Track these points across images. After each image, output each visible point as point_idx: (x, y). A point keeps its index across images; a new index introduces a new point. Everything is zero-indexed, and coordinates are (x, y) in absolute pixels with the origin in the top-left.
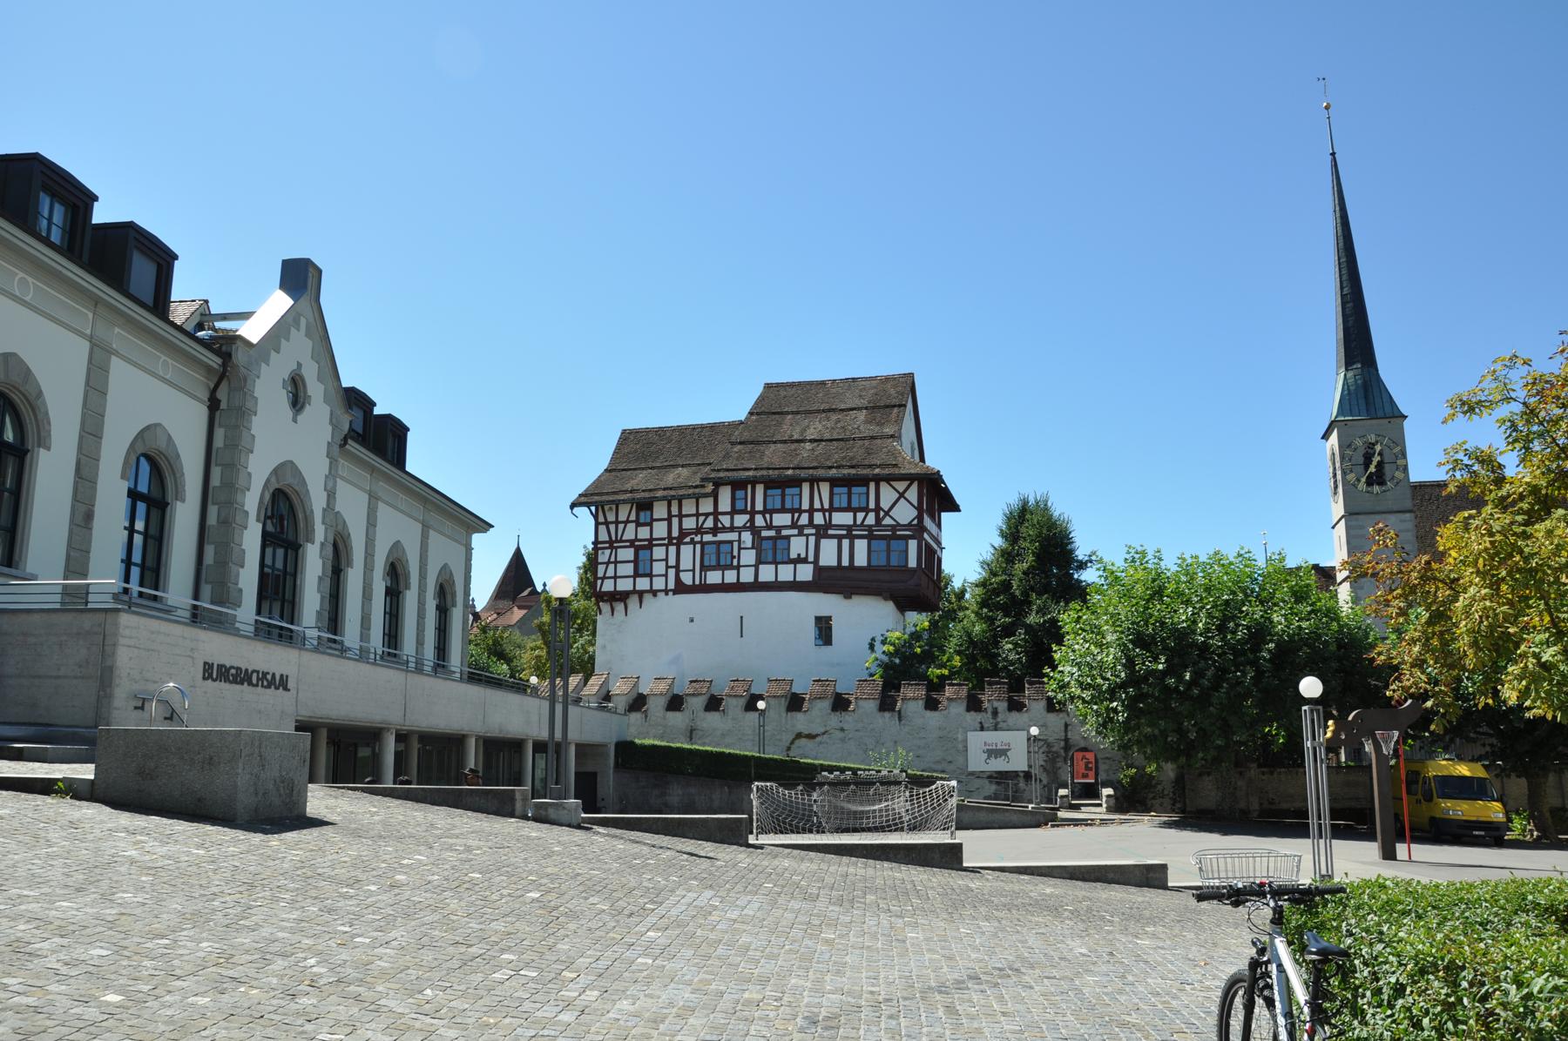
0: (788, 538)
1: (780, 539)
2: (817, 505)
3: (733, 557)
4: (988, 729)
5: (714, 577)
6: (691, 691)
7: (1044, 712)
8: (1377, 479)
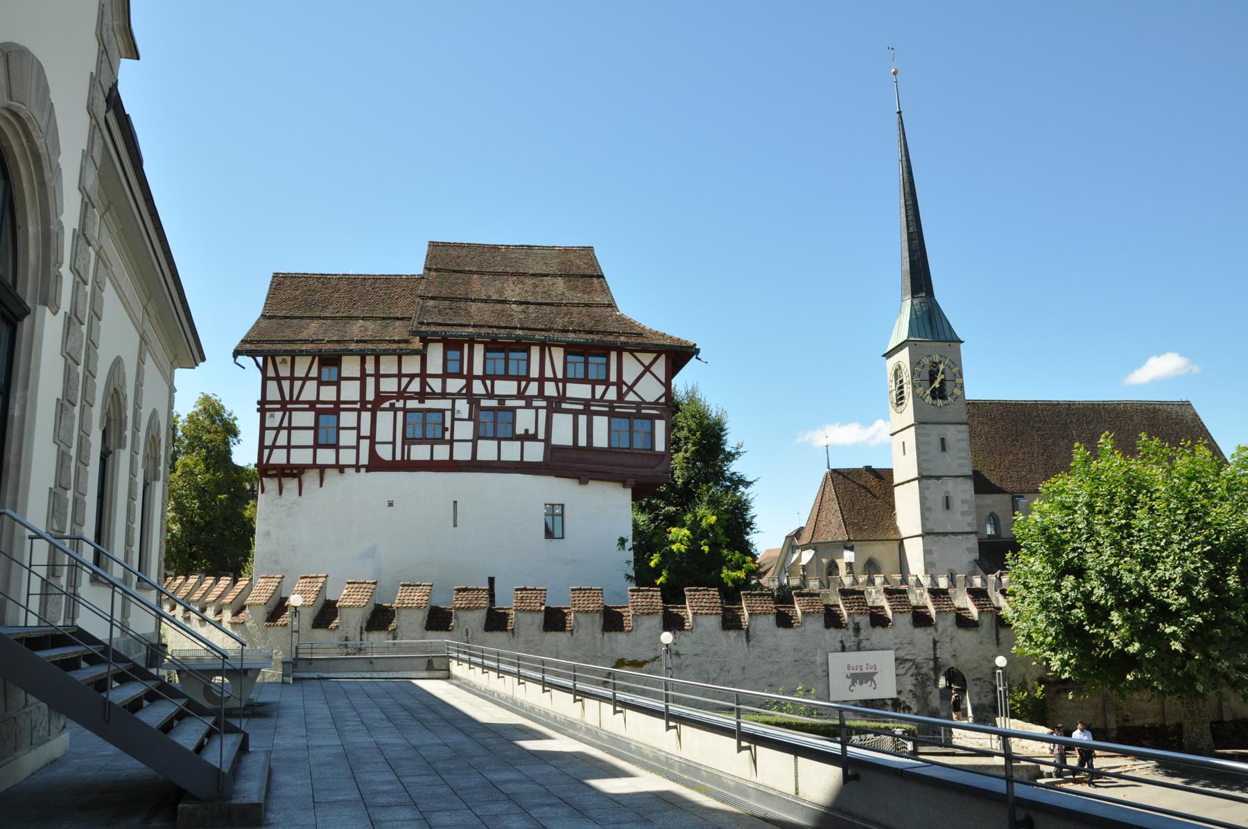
0: (513, 410)
1: (504, 411)
2: (548, 373)
3: (445, 429)
4: (850, 650)
5: (420, 453)
6: (464, 604)
7: (910, 627)
8: (939, 394)
